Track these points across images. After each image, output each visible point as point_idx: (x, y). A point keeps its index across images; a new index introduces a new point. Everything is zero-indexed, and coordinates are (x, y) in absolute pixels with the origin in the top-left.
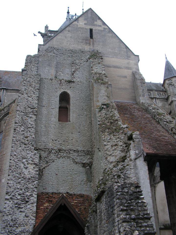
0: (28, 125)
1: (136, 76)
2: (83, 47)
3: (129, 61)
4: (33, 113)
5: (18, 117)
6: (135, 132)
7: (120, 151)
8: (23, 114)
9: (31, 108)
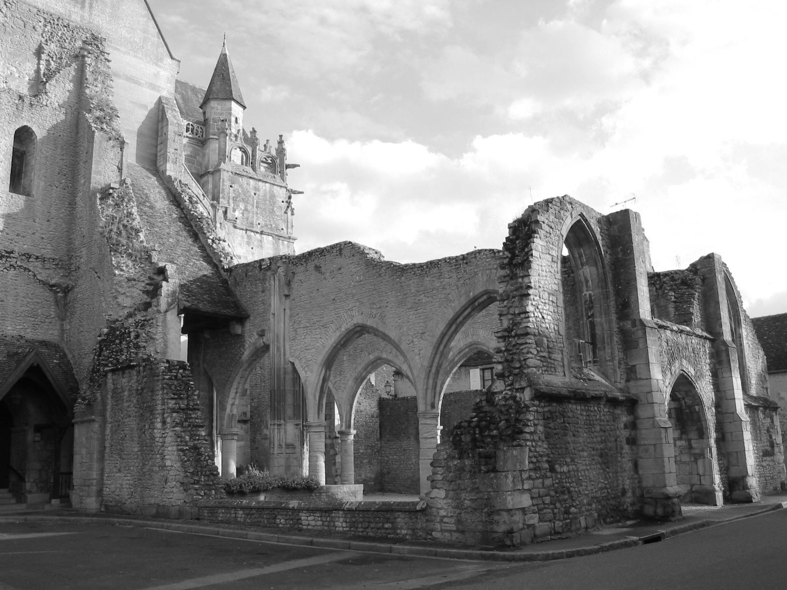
3: (158, 69)
7: (140, 290)
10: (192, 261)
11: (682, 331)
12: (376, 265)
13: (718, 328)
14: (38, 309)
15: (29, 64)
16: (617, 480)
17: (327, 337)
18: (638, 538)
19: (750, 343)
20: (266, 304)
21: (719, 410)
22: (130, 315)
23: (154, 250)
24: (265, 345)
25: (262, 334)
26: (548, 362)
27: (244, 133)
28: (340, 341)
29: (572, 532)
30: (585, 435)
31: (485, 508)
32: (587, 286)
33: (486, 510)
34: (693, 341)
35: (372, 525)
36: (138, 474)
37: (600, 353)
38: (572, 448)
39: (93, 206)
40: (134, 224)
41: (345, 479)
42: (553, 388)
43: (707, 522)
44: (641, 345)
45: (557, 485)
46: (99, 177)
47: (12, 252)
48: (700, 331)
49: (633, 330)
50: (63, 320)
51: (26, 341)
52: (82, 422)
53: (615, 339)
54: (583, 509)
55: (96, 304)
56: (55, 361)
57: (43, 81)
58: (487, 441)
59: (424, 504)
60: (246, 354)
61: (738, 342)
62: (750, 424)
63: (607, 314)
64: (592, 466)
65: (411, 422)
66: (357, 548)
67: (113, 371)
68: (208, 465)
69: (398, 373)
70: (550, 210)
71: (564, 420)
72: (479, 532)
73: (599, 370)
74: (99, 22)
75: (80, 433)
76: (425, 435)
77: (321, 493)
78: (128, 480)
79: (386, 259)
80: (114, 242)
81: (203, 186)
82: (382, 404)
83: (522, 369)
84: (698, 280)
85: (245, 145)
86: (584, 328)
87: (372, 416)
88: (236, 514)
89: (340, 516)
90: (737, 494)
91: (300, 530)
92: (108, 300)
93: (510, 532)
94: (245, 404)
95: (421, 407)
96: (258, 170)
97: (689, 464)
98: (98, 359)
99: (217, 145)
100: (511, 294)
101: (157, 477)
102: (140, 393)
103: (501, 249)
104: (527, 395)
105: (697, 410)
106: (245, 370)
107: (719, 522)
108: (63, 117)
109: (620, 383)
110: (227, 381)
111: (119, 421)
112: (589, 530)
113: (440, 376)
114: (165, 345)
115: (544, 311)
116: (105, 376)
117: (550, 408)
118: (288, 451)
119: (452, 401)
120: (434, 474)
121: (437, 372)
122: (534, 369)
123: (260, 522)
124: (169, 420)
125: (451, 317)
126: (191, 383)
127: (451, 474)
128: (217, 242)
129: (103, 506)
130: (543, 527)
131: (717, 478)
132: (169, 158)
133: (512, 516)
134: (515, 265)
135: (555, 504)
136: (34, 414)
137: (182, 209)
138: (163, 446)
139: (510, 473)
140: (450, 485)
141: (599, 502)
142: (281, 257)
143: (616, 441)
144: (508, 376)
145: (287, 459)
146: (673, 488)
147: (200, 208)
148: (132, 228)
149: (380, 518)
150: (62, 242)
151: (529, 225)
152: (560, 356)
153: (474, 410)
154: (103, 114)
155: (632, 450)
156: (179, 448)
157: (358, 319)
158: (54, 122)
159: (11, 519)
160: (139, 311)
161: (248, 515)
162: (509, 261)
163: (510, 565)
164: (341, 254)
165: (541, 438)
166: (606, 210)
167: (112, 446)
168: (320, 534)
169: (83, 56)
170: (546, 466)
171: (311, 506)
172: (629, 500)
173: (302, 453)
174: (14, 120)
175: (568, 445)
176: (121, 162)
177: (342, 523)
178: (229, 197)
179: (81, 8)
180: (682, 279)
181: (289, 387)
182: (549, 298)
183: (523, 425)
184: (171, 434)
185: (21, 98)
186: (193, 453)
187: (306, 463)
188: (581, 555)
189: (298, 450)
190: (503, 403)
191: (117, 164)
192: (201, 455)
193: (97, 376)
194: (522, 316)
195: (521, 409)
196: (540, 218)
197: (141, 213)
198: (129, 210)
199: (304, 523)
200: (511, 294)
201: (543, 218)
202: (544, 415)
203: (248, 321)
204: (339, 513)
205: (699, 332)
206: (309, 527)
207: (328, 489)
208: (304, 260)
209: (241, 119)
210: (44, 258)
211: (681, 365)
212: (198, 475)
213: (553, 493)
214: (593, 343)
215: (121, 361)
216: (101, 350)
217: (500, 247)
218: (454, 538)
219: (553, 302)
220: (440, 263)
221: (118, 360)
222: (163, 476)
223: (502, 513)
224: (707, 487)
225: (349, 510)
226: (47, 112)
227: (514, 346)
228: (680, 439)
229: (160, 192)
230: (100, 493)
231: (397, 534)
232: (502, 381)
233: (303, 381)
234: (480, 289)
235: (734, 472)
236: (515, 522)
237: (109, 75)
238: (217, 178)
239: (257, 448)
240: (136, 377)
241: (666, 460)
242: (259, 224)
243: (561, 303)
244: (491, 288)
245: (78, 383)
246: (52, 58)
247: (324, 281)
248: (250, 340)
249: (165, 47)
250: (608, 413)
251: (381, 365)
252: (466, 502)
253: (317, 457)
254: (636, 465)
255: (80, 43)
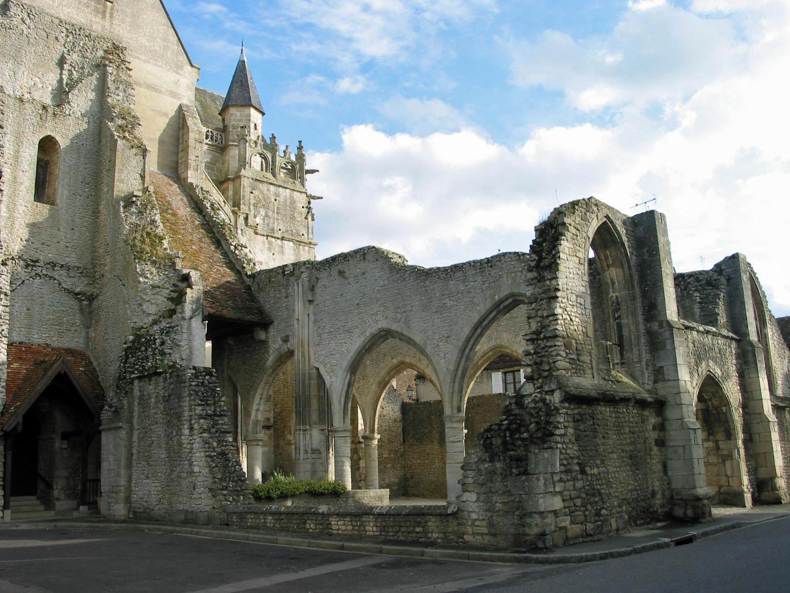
3: (179, 77)
7: (165, 298)
10: (215, 268)
11: (708, 332)
12: (400, 270)
13: (744, 328)
14: (63, 317)
15: (51, 75)
16: (647, 482)
17: (352, 342)
18: (670, 540)
19: (776, 343)
20: (291, 310)
21: (747, 410)
22: (155, 322)
23: (178, 257)
24: (289, 350)
25: (286, 340)
26: (577, 364)
27: (263, 140)
28: (365, 346)
29: (603, 534)
30: (615, 436)
31: (517, 510)
32: (613, 288)
33: (518, 513)
34: (720, 342)
35: (403, 529)
36: (165, 480)
37: (627, 355)
38: (601, 450)
39: (116, 214)
40: (157, 231)
41: (370, 483)
42: (583, 391)
43: (737, 524)
44: (668, 346)
45: (587, 487)
46: (122, 184)
47: (37, 261)
48: (726, 331)
49: (660, 331)
50: (88, 328)
51: (53, 349)
52: (109, 429)
53: (643, 340)
54: (614, 511)
55: (120, 311)
56: (81, 369)
57: (66, 91)
58: (517, 444)
59: (454, 507)
60: (271, 360)
61: (764, 342)
62: (778, 425)
63: (634, 315)
64: (622, 468)
65: (435, 426)
66: (389, 552)
67: (139, 378)
68: (235, 471)
69: (421, 377)
70: (577, 212)
71: (593, 423)
72: (512, 535)
73: (627, 372)
74: (119, 31)
75: (107, 440)
76: (451, 438)
77: (348, 498)
78: (156, 486)
79: (410, 263)
80: (138, 249)
81: (224, 192)
82: (405, 408)
83: (551, 371)
84: (723, 280)
85: (264, 151)
86: (610, 329)
87: (395, 421)
88: (265, 519)
89: (371, 520)
90: (765, 495)
91: (331, 535)
92: (133, 307)
93: (543, 535)
94: (268, 409)
95: (447, 411)
96: (278, 176)
97: (716, 465)
98: (124, 367)
99: (237, 152)
100: (539, 297)
101: (184, 483)
102: (167, 399)
103: (528, 252)
104: (557, 397)
105: (724, 411)
106: (270, 376)
107: (749, 524)
108: (85, 126)
109: (648, 384)
110: (251, 387)
111: (147, 428)
112: (620, 532)
113: (466, 380)
114: (190, 352)
115: (573, 314)
116: (132, 383)
117: (580, 410)
118: (314, 456)
119: (474, 404)
120: (465, 477)
121: (463, 375)
122: (564, 372)
123: (290, 527)
124: (196, 426)
125: (476, 321)
126: (218, 389)
127: (482, 477)
128: (240, 248)
129: (131, 513)
130: (575, 530)
131: (745, 480)
132: (191, 165)
133: (544, 519)
134: (542, 268)
135: (586, 506)
136: (60, 421)
137: (204, 216)
138: (191, 452)
139: (541, 475)
140: (481, 488)
141: (629, 504)
142: (304, 263)
143: (645, 442)
144: (538, 379)
145: (313, 464)
146: (703, 489)
147: (222, 215)
148: (156, 236)
149: (411, 522)
150: (86, 250)
151: (556, 228)
152: (589, 358)
153: (504, 413)
154: (125, 122)
155: (661, 452)
156: (207, 454)
157: (383, 324)
158: (77, 131)
159: (42, 526)
160: (164, 318)
161: (277, 520)
162: (536, 264)
163: (544, 567)
164: (364, 259)
165: (572, 440)
166: (631, 212)
167: (139, 453)
168: (351, 538)
169: (105, 66)
170: (577, 468)
171: (341, 511)
172: (658, 502)
173: (327, 458)
174: (37, 130)
175: (598, 447)
176: (144, 170)
177: (373, 527)
178: (250, 203)
179: (102, 18)
180: (707, 279)
181: (314, 392)
182: (577, 300)
183: (554, 428)
184: (198, 440)
185: (44, 108)
186: (220, 459)
187: (332, 468)
188: (614, 557)
189: (324, 455)
190: (533, 405)
191: (140, 172)
192: (229, 461)
193: (123, 384)
194: (551, 318)
195: (551, 411)
196: (567, 220)
197: (165, 221)
198: (153, 218)
199: (334, 528)
200: (539, 297)
201: (569, 220)
202: (574, 418)
203: (272, 327)
204: (369, 518)
205: (725, 332)
206: (339, 532)
207: (354, 493)
208: (327, 265)
209: (260, 125)
210: (69, 266)
211: (708, 365)
212: (226, 481)
213: (584, 495)
214: (621, 344)
215: (146, 368)
216: (127, 357)
217: (527, 250)
218: (486, 541)
219: (581, 304)
220: (464, 266)
221: (143, 367)
222: (191, 482)
223: (534, 515)
224: (736, 488)
225: (380, 514)
226: (70, 121)
227: (543, 348)
228: (707, 440)
229: (182, 200)
230: (128, 500)
231: (429, 538)
232: (531, 384)
233: (328, 385)
234: (505, 293)
235: (763, 473)
236: (547, 525)
237: (130, 83)
238: (238, 185)
239: (280, 454)
240: (162, 384)
241: (695, 461)
242: (280, 230)
243: (588, 305)
244: (516, 291)
245: (103, 390)
246: (74, 68)
247: (348, 286)
248: (274, 346)
249: (184, 55)
250: (637, 415)
251: (404, 369)
252: (498, 504)
253: (343, 462)
254: (665, 466)
255: (102, 52)
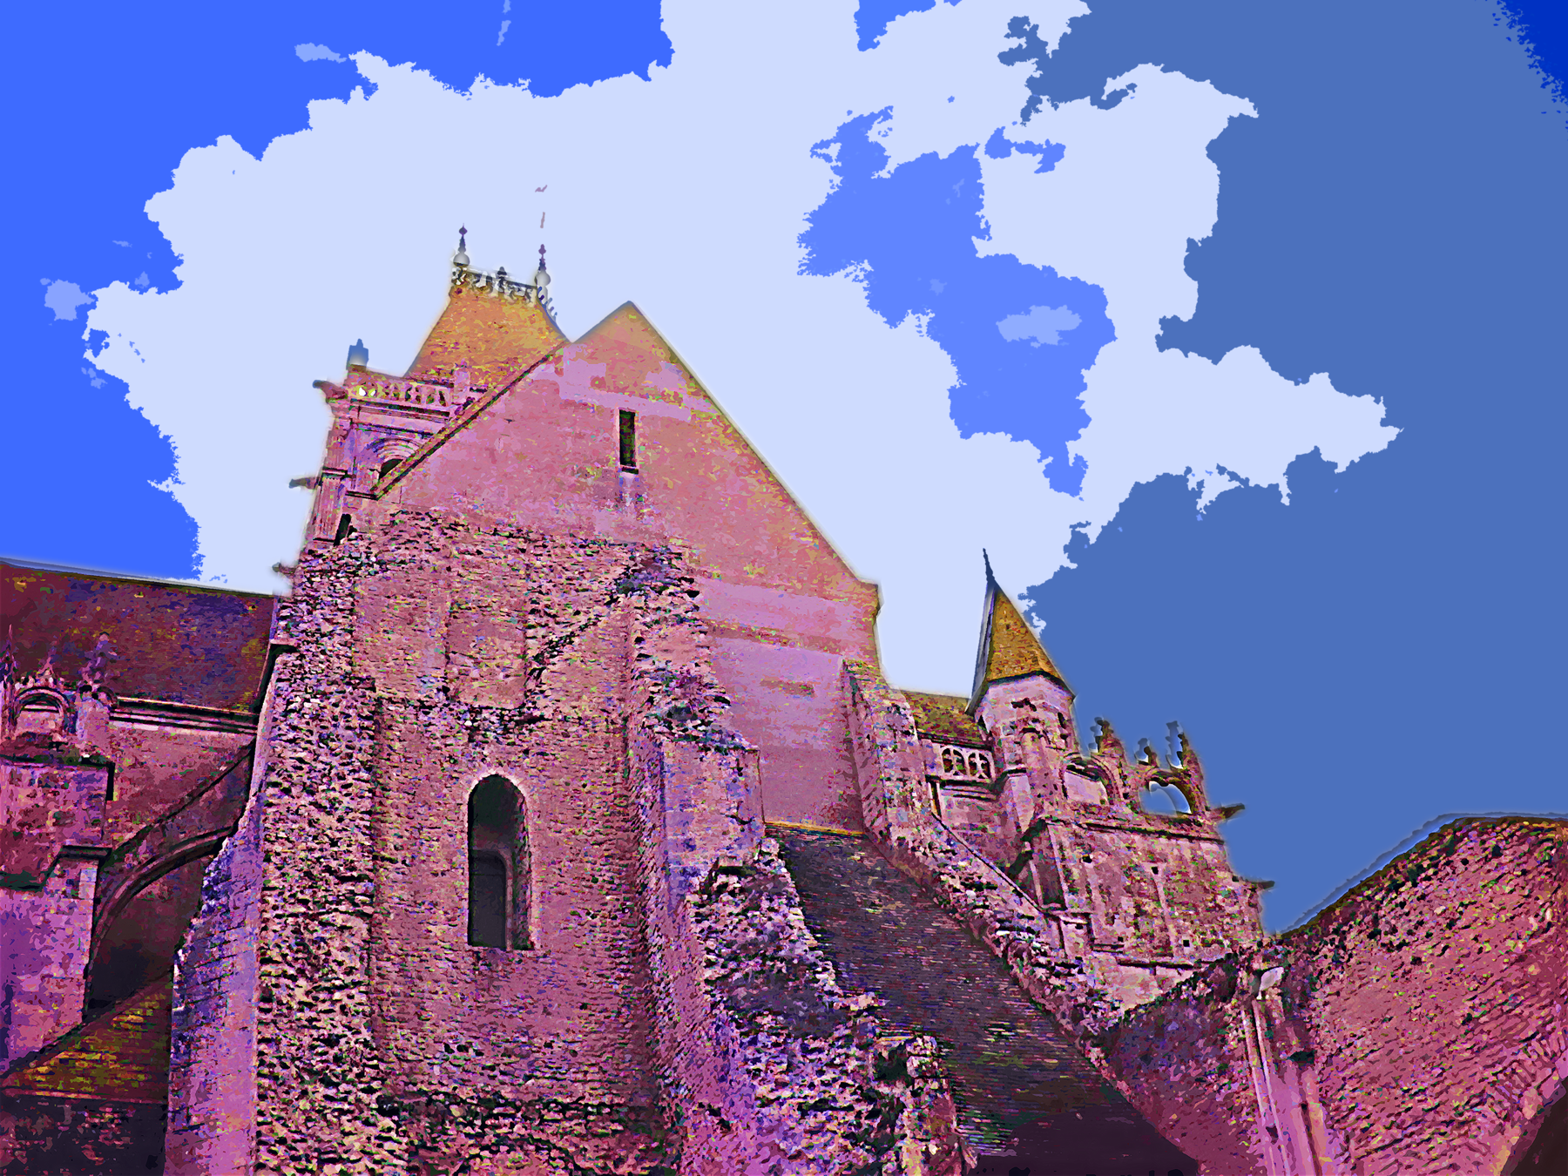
0: (333, 971)
1: (866, 694)
2: (584, 518)
4: (355, 905)
5: (277, 928)
6: (920, 1041)
8: (303, 910)
9: (337, 877)
10: (992, 1033)
